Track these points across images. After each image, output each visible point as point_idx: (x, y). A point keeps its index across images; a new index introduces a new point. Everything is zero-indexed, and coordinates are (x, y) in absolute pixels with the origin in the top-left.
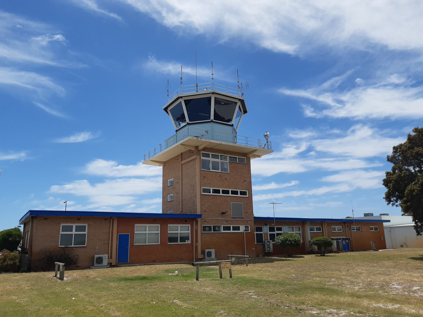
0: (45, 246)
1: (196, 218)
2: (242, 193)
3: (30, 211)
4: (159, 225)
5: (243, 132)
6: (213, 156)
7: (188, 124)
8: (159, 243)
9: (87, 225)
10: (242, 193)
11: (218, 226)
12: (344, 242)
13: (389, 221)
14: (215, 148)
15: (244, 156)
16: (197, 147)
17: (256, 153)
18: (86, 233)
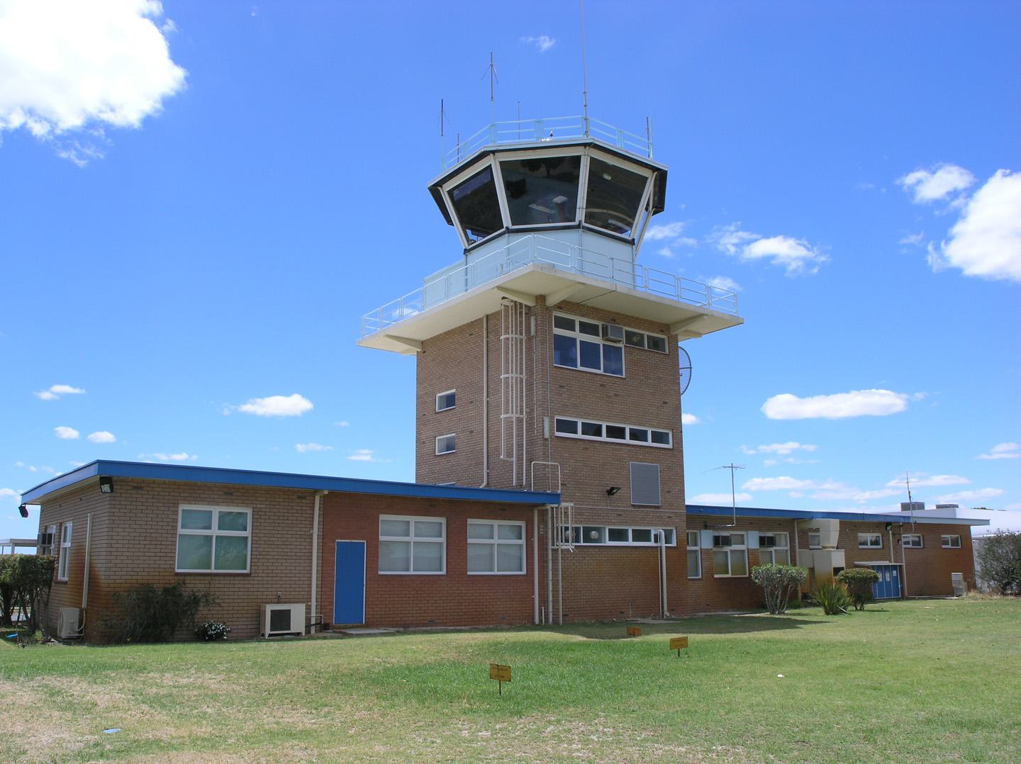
0: (134, 572)
1: (544, 504)
2: (658, 437)
3: (99, 462)
4: (443, 520)
5: (656, 259)
6: (585, 328)
7: (509, 231)
8: (444, 572)
9: (249, 511)
10: (658, 437)
11: (594, 529)
12: (887, 575)
13: (986, 522)
14: (590, 303)
15: (662, 331)
16: (541, 298)
17: (693, 327)
18: (247, 533)
